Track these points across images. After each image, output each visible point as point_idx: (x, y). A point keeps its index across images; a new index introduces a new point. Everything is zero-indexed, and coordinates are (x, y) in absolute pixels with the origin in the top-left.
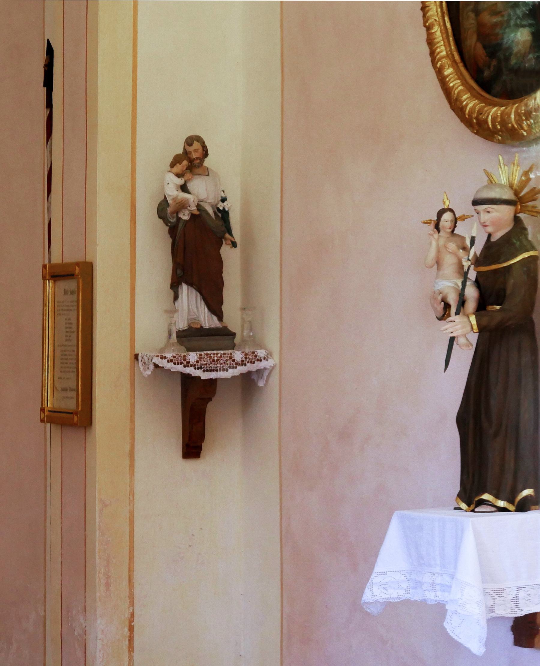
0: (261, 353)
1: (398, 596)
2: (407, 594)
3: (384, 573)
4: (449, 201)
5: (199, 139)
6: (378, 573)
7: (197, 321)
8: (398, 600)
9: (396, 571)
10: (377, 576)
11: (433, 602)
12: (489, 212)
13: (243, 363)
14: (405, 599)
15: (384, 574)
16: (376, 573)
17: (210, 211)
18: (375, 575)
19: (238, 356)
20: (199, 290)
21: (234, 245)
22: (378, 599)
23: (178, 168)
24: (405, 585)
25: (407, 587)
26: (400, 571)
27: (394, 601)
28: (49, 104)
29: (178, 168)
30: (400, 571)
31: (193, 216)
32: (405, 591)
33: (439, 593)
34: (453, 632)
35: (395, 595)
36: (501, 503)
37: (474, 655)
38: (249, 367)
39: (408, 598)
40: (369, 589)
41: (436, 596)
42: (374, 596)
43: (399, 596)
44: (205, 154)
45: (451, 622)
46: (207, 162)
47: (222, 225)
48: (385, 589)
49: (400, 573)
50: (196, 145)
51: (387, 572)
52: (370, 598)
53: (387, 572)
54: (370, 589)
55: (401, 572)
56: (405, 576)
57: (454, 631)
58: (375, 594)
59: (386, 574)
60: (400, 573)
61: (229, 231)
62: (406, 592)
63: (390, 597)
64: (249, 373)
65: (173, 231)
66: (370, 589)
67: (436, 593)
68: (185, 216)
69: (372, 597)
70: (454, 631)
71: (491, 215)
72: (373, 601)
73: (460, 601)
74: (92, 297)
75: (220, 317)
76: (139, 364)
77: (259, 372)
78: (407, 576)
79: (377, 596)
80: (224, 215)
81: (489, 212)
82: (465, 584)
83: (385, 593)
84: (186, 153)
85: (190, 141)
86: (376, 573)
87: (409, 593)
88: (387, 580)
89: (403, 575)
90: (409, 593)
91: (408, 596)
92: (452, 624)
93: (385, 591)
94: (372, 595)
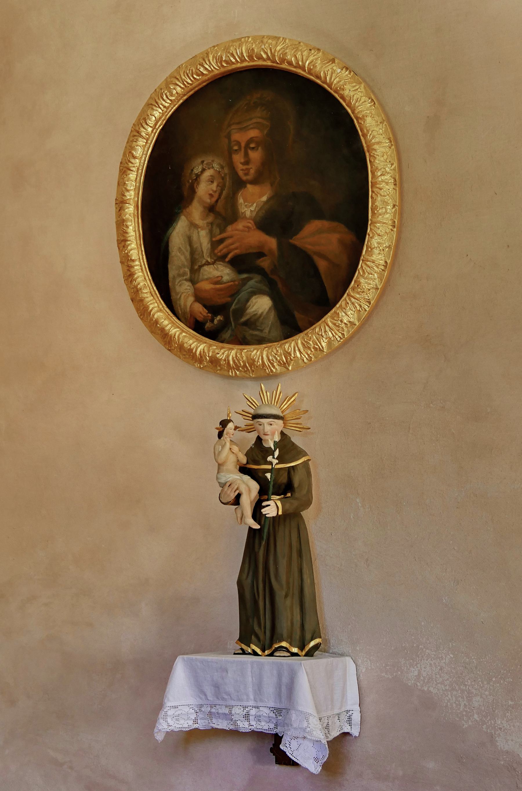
1: (188, 726)
2: (196, 723)
3: (176, 707)
6: (170, 707)
8: (188, 729)
9: (185, 705)
10: (252, 709)
11: (247, 730)
12: (271, 425)
14: (194, 728)
15: (176, 708)
16: (169, 707)
18: (169, 708)
22: (174, 728)
24: (193, 717)
25: (195, 718)
26: (189, 705)
27: (268, 732)
30: (189, 705)
32: (194, 722)
33: (253, 723)
34: (292, 755)
35: (266, 727)
36: (295, 650)
37: (312, 774)
39: (197, 727)
40: (348, 724)
41: (251, 725)
42: (251, 725)
43: (189, 726)
45: (290, 746)
48: (177, 720)
49: (189, 707)
51: (178, 706)
52: (167, 728)
53: (178, 706)
54: (165, 721)
55: (190, 706)
56: (193, 709)
57: (292, 753)
58: (252, 724)
59: (178, 708)
60: (189, 707)
62: (195, 722)
63: (182, 727)
66: (165, 721)
67: (250, 723)
69: (168, 727)
70: (292, 753)
71: (272, 426)
72: (169, 730)
73: (308, 729)
78: (195, 709)
79: (172, 726)
81: (271, 425)
82: (308, 715)
83: (178, 724)
86: (169, 707)
87: (197, 723)
88: (179, 712)
89: (191, 708)
90: (197, 723)
91: (196, 726)
92: (291, 748)
93: (259, 723)
94: (168, 726)
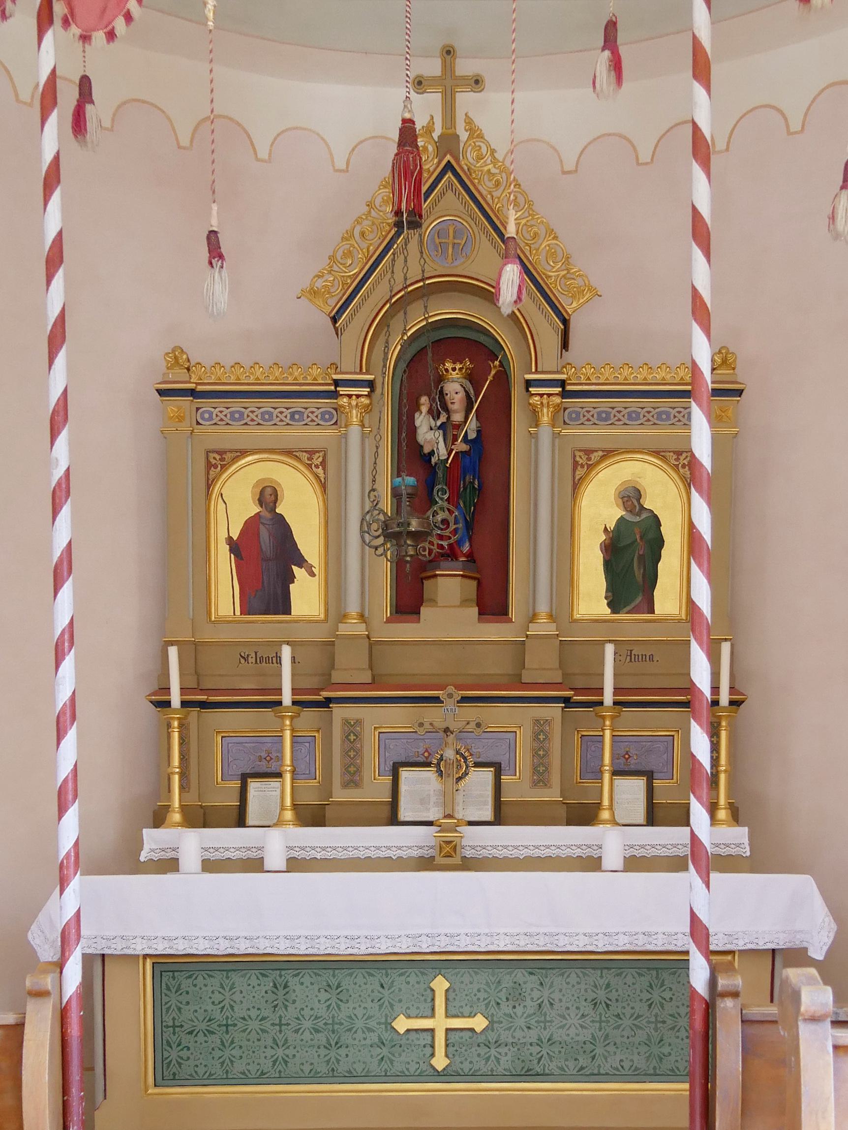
4: (17, 95)
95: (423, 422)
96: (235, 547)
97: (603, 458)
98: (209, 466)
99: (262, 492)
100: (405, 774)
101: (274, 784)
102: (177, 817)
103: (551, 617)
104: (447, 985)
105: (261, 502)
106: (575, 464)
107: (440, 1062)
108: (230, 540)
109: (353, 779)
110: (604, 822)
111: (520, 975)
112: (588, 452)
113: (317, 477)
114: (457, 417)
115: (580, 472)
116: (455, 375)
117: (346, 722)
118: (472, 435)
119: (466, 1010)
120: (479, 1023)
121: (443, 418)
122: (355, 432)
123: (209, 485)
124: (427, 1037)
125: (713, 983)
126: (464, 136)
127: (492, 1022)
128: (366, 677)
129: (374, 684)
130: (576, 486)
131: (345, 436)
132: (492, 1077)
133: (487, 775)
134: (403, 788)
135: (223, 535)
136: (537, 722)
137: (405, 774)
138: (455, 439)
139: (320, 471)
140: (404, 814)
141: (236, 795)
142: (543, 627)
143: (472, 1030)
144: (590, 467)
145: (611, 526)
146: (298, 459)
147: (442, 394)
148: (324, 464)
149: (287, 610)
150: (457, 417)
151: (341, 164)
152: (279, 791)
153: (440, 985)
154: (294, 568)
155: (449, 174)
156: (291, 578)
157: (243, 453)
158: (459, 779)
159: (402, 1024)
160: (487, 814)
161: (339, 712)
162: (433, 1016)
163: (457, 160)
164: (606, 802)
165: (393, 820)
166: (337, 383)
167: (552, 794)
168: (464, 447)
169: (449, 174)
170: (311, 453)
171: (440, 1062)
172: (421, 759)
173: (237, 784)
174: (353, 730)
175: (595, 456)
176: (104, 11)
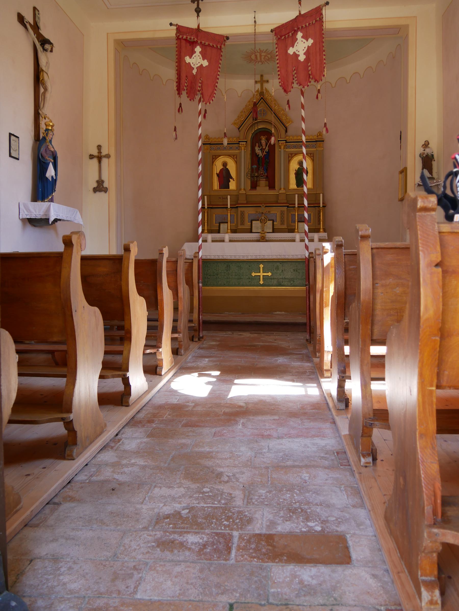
0: (440, 181)
5: (427, 141)
7: (222, 392)
13: (436, 183)
17: (430, 155)
19: (435, 181)
20: (427, 170)
21: (434, 161)
23: (423, 147)
28: (401, 143)
29: (423, 147)
31: (426, 156)
38: (437, 183)
44: (429, 144)
46: (429, 146)
47: (341, 598)
50: (427, 142)
61: (433, 158)
64: (437, 185)
65: (422, 158)
68: (424, 156)
74: (314, 166)
75: (432, 175)
76: (108, 442)
77: (439, 184)
80: (433, 155)
84: (425, 144)
85: (425, 142)
95: (257, 149)
96: (218, 175)
97: (295, 155)
98: (213, 158)
99: (224, 164)
100: (254, 222)
101: (226, 224)
102: (206, 231)
103: (284, 189)
104: (263, 266)
105: (223, 165)
106: (289, 157)
107: (261, 282)
108: (217, 174)
109: (242, 224)
110: (296, 232)
111: (278, 264)
112: (292, 154)
113: (235, 160)
114: (264, 147)
115: (290, 158)
116: (263, 139)
117: (241, 211)
118: (267, 151)
119: (267, 271)
120: (270, 274)
121: (261, 148)
122: (243, 151)
123: (213, 162)
124: (259, 277)
125: (309, 256)
126: (265, 92)
127: (272, 274)
128: (245, 202)
129: (247, 204)
130: (289, 161)
131: (241, 152)
132: (272, 286)
133: (271, 222)
134: (253, 225)
135: (215, 173)
136: (281, 211)
137: (254, 222)
138: (264, 152)
139: (236, 159)
140: (253, 231)
141: (218, 227)
142: (282, 191)
143: (268, 276)
144: (292, 157)
145: (297, 169)
146: (231, 157)
147: (261, 143)
148: (236, 158)
149: (229, 188)
150: (264, 147)
151: (239, 95)
152: (227, 227)
153: (262, 266)
154: (230, 179)
155: (262, 100)
156: (230, 181)
157: (220, 156)
158: (265, 223)
159: (254, 274)
160: (271, 231)
161: (240, 209)
162: (260, 273)
163: (264, 97)
164: (296, 228)
165: (251, 232)
166: (239, 142)
167: (285, 227)
168: (265, 154)
169: (262, 100)
170: (234, 156)
171: (261, 282)
172: (257, 219)
173: (218, 225)
174: (242, 213)
175: (293, 155)
176: (209, 100)
